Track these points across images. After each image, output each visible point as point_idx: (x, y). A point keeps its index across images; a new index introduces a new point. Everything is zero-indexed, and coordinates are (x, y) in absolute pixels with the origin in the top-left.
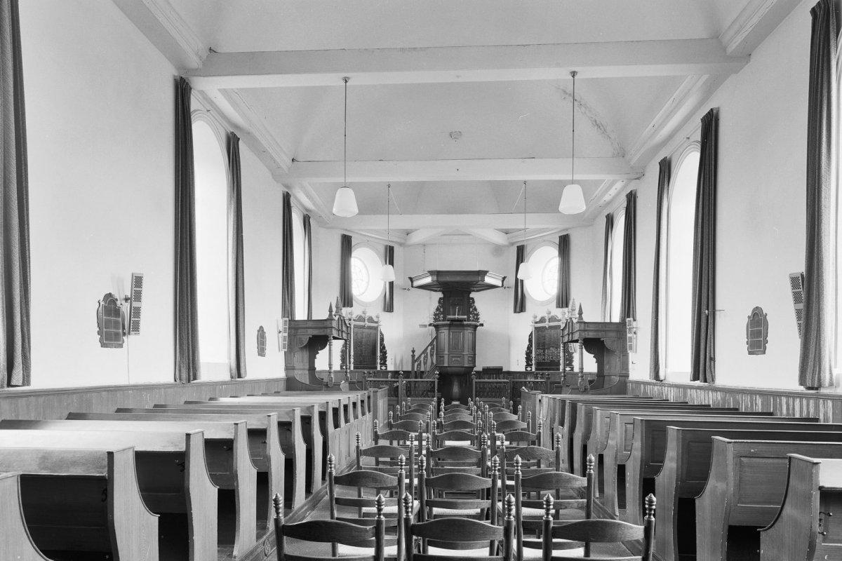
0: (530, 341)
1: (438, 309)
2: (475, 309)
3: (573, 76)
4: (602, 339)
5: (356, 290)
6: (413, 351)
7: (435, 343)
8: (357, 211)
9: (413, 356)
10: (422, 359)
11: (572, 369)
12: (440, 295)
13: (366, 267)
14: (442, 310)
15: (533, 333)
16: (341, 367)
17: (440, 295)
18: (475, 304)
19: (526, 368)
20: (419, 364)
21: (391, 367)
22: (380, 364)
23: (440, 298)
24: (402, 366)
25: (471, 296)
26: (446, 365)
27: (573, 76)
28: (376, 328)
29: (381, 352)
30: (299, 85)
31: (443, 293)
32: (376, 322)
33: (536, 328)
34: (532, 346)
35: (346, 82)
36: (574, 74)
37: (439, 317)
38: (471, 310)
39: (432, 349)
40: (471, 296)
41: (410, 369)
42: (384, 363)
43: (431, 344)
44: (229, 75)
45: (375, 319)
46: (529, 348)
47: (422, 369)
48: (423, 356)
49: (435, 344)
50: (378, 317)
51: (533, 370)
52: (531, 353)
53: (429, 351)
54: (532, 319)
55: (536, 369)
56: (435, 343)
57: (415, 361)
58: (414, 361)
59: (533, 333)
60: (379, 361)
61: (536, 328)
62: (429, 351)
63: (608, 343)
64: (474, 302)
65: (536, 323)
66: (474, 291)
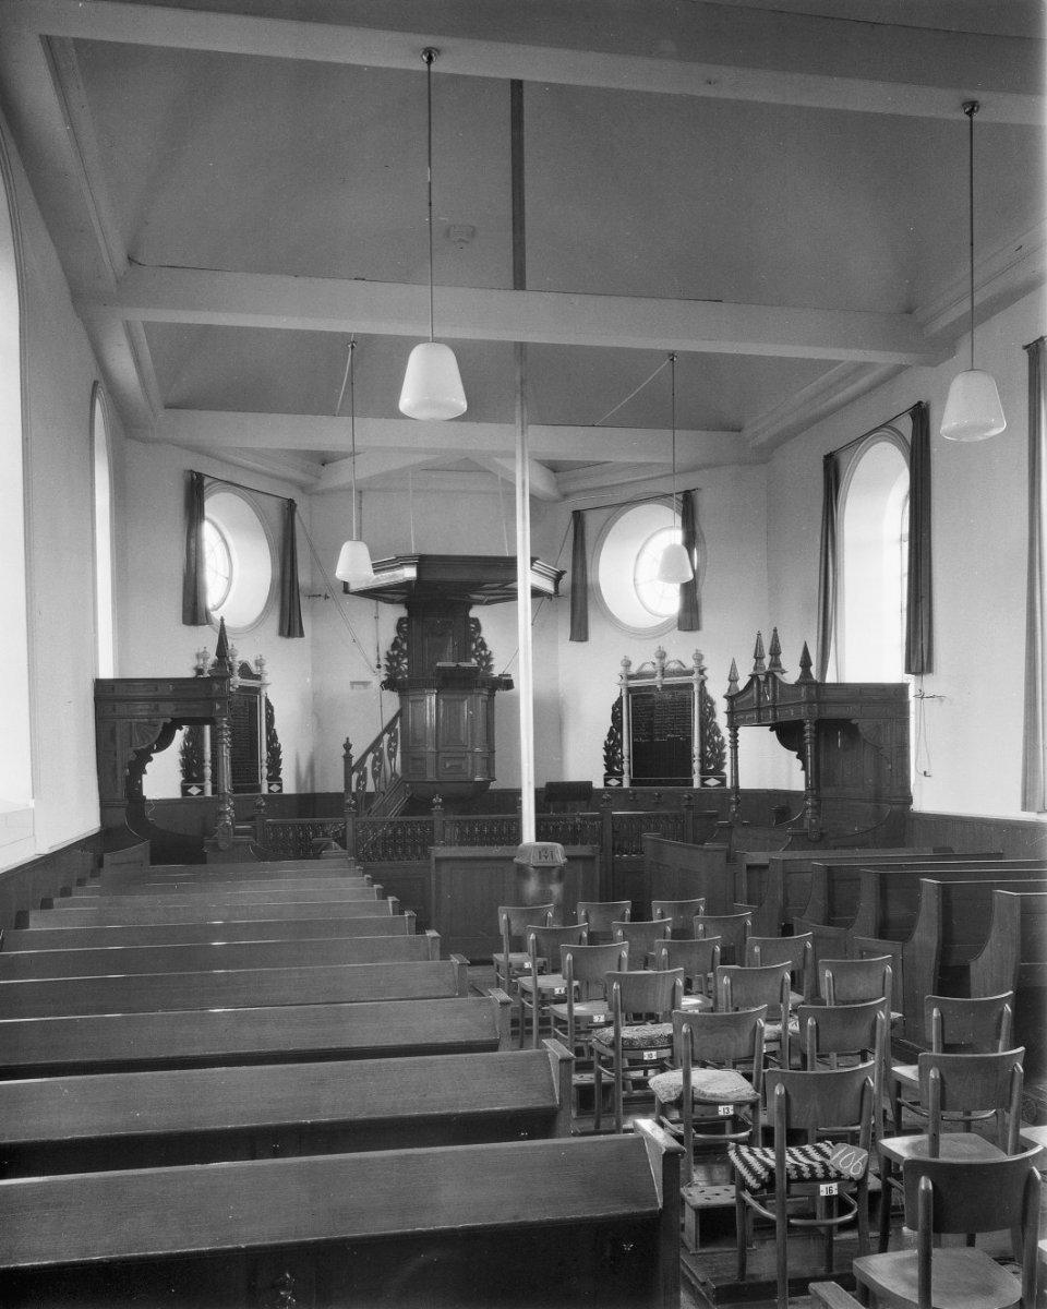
0: (616, 717)
1: (395, 645)
2: (483, 646)
3: (970, 114)
4: (853, 722)
5: (214, 592)
6: (348, 746)
7: (398, 726)
8: (464, 405)
9: (348, 758)
10: (368, 764)
11: (723, 782)
12: (402, 612)
13: (224, 540)
14: (405, 647)
15: (624, 699)
16: (184, 790)
17: (402, 612)
18: (483, 635)
19: (606, 780)
20: (362, 778)
21: (289, 787)
22: (269, 778)
23: (401, 620)
24: (313, 780)
25: (473, 613)
26: (431, 776)
27: (970, 114)
28: (257, 691)
29: (268, 749)
30: (614, 85)
31: (407, 607)
32: (258, 677)
33: (630, 690)
34: (620, 729)
35: (430, 59)
36: (972, 108)
37: (399, 664)
38: (474, 647)
39: (394, 739)
40: (473, 613)
41: (341, 789)
42: (275, 777)
43: (389, 728)
44: (201, 10)
45: (254, 669)
46: (615, 733)
47: (370, 788)
48: (371, 757)
49: (401, 729)
50: (259, 663)
51: (626, 785)
52: (621, 746)
53: (384, 745)
54: (621, 669)
55: (632, 783)
56: (398, 726)
57: (353, 770)
58: (349, 769)
59: (624, 699)
60: (265, 771)
61: (630, 690)
62: (384, 745)
63: (865, 726)
64: (478, 628)
65: (630, 677)
66: (480, 603)
